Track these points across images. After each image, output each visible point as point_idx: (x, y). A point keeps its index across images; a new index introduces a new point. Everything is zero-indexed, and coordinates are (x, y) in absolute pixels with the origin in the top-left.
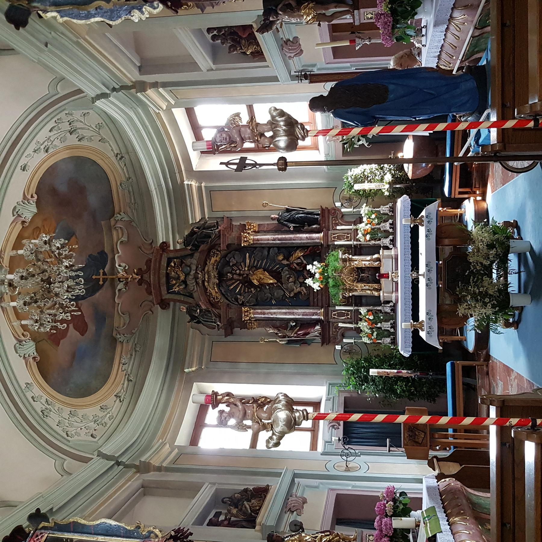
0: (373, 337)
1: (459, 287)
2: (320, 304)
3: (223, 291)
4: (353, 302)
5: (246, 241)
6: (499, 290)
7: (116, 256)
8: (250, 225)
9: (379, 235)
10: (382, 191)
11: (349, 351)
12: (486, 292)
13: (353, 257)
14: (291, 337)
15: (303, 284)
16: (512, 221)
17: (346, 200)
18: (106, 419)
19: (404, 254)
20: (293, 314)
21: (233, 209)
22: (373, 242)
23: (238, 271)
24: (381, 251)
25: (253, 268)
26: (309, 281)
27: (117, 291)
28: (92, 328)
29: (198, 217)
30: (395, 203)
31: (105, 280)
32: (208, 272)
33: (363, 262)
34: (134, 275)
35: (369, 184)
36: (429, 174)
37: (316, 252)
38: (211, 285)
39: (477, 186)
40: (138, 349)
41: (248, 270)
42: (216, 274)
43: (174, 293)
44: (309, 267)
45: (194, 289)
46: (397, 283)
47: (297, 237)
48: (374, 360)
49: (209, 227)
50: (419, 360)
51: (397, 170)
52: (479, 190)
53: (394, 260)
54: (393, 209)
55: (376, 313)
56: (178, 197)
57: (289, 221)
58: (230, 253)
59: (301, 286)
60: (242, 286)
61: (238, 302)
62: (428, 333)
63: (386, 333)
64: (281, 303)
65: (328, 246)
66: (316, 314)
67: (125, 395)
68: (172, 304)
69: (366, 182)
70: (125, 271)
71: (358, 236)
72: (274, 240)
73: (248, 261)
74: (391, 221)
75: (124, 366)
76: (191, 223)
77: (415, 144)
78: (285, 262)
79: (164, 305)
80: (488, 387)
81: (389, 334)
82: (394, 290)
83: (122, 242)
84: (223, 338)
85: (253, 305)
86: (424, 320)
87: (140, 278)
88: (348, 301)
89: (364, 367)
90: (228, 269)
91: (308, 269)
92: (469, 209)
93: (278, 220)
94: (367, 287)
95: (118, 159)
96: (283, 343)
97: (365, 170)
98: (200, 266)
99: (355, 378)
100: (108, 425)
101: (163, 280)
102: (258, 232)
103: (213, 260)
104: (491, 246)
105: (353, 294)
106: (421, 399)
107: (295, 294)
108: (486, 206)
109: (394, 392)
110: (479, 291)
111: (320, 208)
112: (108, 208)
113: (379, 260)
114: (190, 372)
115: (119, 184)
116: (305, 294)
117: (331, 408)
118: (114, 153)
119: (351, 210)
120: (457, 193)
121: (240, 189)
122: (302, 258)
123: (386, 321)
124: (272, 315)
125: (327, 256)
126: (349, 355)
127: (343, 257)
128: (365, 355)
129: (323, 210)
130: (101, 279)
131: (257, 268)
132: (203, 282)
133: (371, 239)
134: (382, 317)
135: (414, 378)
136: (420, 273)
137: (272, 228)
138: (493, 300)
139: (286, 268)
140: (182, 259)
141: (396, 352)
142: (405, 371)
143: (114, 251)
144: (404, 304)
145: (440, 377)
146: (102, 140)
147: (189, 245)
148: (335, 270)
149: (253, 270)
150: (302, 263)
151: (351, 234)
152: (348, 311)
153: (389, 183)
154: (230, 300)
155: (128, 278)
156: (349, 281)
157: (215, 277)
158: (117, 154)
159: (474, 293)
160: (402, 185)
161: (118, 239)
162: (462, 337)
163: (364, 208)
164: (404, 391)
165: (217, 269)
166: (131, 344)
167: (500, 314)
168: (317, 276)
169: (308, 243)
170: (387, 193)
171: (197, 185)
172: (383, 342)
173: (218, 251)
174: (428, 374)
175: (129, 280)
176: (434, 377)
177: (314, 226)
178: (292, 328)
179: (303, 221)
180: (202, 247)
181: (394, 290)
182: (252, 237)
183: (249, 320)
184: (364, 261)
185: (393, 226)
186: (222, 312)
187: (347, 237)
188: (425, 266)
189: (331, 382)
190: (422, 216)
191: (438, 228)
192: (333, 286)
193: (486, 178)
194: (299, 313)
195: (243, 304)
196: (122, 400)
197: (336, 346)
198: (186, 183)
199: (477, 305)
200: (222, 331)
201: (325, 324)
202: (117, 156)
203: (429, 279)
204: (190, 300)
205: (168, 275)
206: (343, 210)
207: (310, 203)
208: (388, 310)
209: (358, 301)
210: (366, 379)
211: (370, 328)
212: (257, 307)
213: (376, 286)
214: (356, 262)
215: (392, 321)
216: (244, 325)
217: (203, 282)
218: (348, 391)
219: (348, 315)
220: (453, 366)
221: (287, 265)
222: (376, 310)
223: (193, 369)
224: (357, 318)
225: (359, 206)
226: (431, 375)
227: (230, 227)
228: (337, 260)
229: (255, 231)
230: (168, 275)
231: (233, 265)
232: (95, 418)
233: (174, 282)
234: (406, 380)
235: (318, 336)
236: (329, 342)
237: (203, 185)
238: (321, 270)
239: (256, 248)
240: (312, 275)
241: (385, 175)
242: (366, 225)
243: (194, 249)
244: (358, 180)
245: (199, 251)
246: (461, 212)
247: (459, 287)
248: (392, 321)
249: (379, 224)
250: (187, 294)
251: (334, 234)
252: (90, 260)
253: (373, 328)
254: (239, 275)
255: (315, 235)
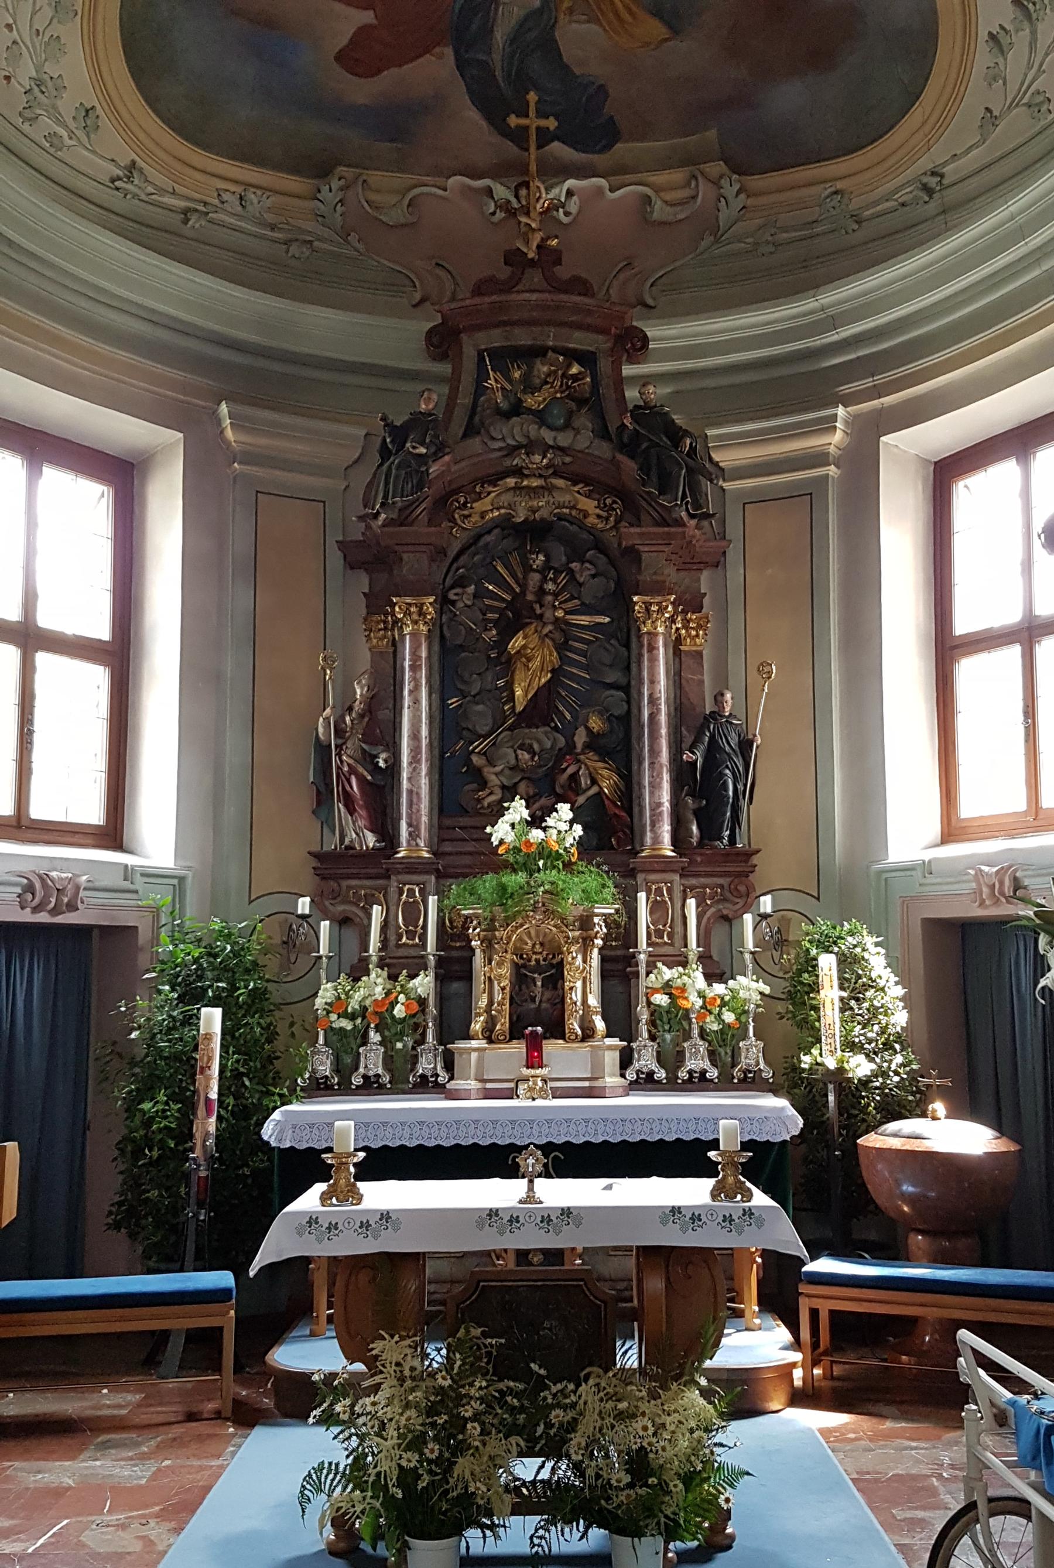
0: (333, 1017)
1: (484, 1335)
2: (447, 847)
3: (488, 538)
4: (455, 954)
5: (648, 610)
6: (467, 1498)
7: (602, 182)
8: (700, 627)
9: (668, 1037)
10: (813, 1045)
11: (294, 941)
12: (461, 1448)
13: (596, 951)
14: (339, 755)
15: (510, 793)
16: (729, 1531)
17: (779, 931)
18: (47, 123)
19: (606, 1117)
20: (415, 760)
21: (750, 572)
22: (645, 1017)
23: (550, 586)
24: (615, 1041)
25: (564, 638)
26: (518, 810)
27: (486, 182)
28: (361, 91)
29: (724, 458)
30: (775, 1091)
31: (519, 137)
32: (549, 489)
33: (579, 984)
34: (537, 238)
35: (837, 1004)
36: (872, 1201)
37: (611, 834)
38: (506, 498)
39: (837, 1370)
40: (294, 249)
41: (557, 619)
42: (543, 513)
43: (482, 375)
44: (565, 811)
45: (493, 439)
46: (511, 1094)
47: (660, 775)
48: (255, 1025)
49: (693, 488)
50: (255, 1173)
51: (883, 1095)
52: (825, 1377)
53: (586, 1084)
54: (751, 1082)
55: (414, 1025)
56: (796, 385)
57: (713, 749)
58: (612, 562)
59: (503, 787)
60: (503, 600)
61: (452, 587)
62: (312, 1220)
63: (348, 1060)
64: (449, 727)
65: (631, 873)
66: (413, 835)
67: (135, 196)
68: (445, 368)
69: (845, 994)
70: (555, 206)
71: (665, 969)
72: (653, 701)
73: (584, 620)
74: (713, 1073)
75: (234, 200)
76: (709, 433)
77: (979, 1157)
78: (581, 738)
79: (442, 341)
80: (144, 1418)
81: (344, 1069)
82: (489, 1085)
83: (647, 200)
84: (334, 537)
85: (442, 637)
86: (367, 1204)
87: (531, 255)
88: (453, 934)
89: (234, 988)
90: (560, 557)
91: (559, 806)
92: (757, 1344)
93: (715, 715)
94: (498, 997)
95: (925, 180)
96: (321, 730)
97: (883, 989)
98: (568, 459)
99: (196, 961)
100: (26, 127)
101: (523, 338)
102: (677, 652)
103: (589, 505)
104: (639, 1464)
105: (478, 952)
106: (125, 1183)
107: (479, 771)
108: (774, 1406)
109: (146, 1091)
110: (466, 1420)
111: (754, 846)
112: (760, 152)
113: (588, 1033)
114: (219, 422)
115: (839, 185)
116: (479, 800)
117: (97, 884)
118: (945, 164)
119: (750, 944)
120: (817, 1303)
121: (814, 591)
122: (594, 790)
123: (389, 1061)
124: (411, 692)
125: (598, 866)
126: (277, 940)
127: (596, 920)
128: (276, 993)
129: (748, 855)
130: (523, 121)
131: (562, 648)
132: (518, 472)
133: (655, 1011)
134: (399, 1045)
135: (187, 1159)
136: (539, 1182)
137: (691, 696)
138: (431, 1472)
139: (562, 741)
140: (591, 402)
141: (281, 1096)
142: (212, 1129)
143: (616, 172)
144: (440, 1119)
145: (191, 1246)
146: (990, 117)
147: (635, 419)
148: (554, 893)
149: (557, 635)
150: (578, 791)
151: (672, 944)
152: (423, 937)
153: (841, 1070)
154: (463, 559)
155: (527, 214)
156: (520, 939)
157: (534, 512)
158: (942, 176)
159: (460, 1400)
160: (838, 1114)
161: (658, 190)
162: (323, 1319)
163: (754, 985)
164: (148, 1123)
165: (560, 518)
166: (309, 225)
167: (378, 1505)
168: (536, 835)
169: (642, 809)
170: (806, 1061)
171: (832, 449)
172: (319, 1052)
173: (617, 522)
174: (200, 1205)
175: (524, 219)
176: (192, 1227)
177: (694, 828)
178: (369, 760)
179: (711, 792)
180: (630, 466)
181: (489, 1085)
182: (660, 630)
183: (396, 621)
184: (584, 988)
185: (698, 1082)
186: (421, 529)
187: (660, 934)
188: (565, 1204)
189: (189, 881)
190: (749, 1196)
191: (705, 1254)
192: (503, 888)
193: (871, 1408)
194: (416, 782)
195: (444, 602)
196: (118, 184)
197: (308, 899)
198: (841, 411)
199: (412, 1413)
200: (357, 533)
201: (380, 865)
202: (933, 174)
203: (514, 1220)
204: (457, 428)
205: (539, 352)
206: (748, 918)
207: (769, 815)
208: (425, 1065)
209: (454, 970)
210: (192, 996)
211: (365, 1009)
212: (436, 648)
213: (503, 1025)
214: (579, 960)
215: (386, 1079)
216: (377, 604)
217: (518, 472)
218: (156, 941)
219: (411, 935)
220: (219, 1296)
221: (571, 746)
222: (426, 1027)
223: (229, 434)
224: (399, 964)
225: (761, 972)
226: (196, 1215)
227: (694, 562)
228: (588, 899)
229: (679, 640)
230: (539, 352)
231: (571, 572)
232: (50, 84)
233: (517, 375)
234: (184, 1133)
235: (342, 842)
236: (324, 878)
237: (832, 470)
238: (555, 847)
239: (627, 645)
240: (536, 821)
241: (867, 1056)
242: (701, 995)
243: (625, 440)
244: (849, 963)
245: (620, 457)
246: (747, 1314)
247: (484, 1335)
248: (386, 1079)
249: (703, 1034)
250: (477, 419)
251: (669, 890)
252: (591, 90)
253: (364, 1017)
254: (541, 592)
255: (666, 830)
